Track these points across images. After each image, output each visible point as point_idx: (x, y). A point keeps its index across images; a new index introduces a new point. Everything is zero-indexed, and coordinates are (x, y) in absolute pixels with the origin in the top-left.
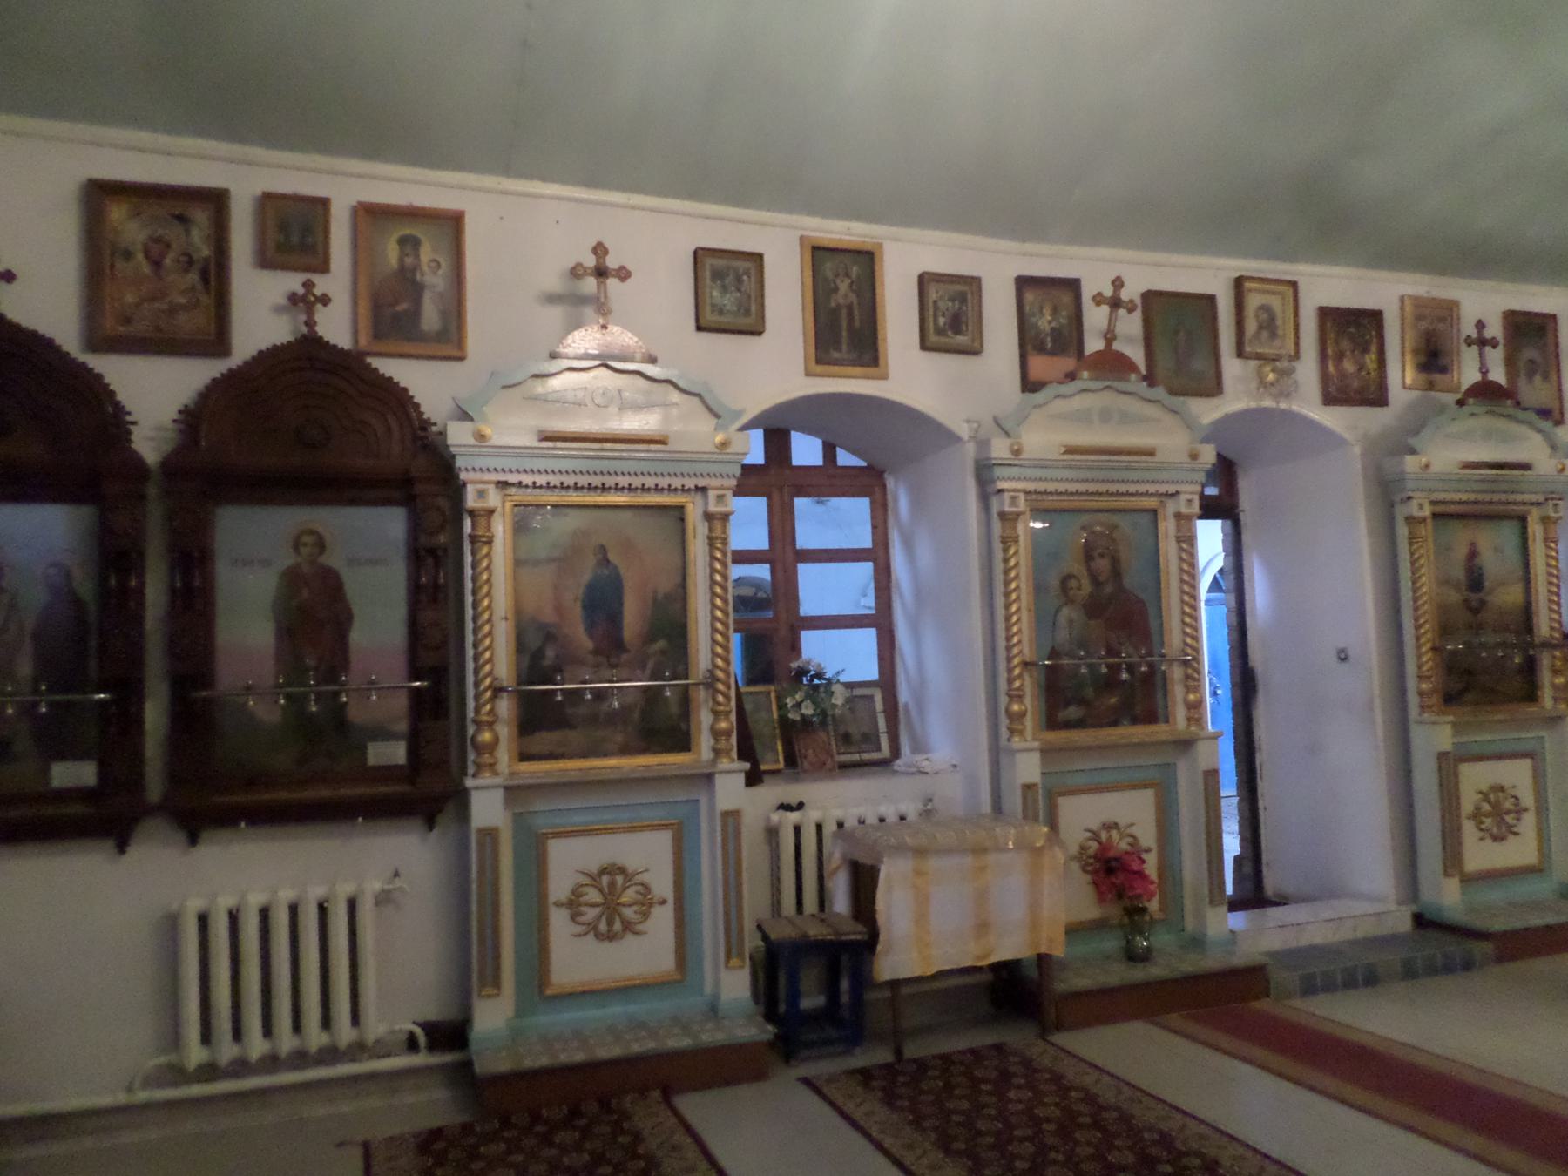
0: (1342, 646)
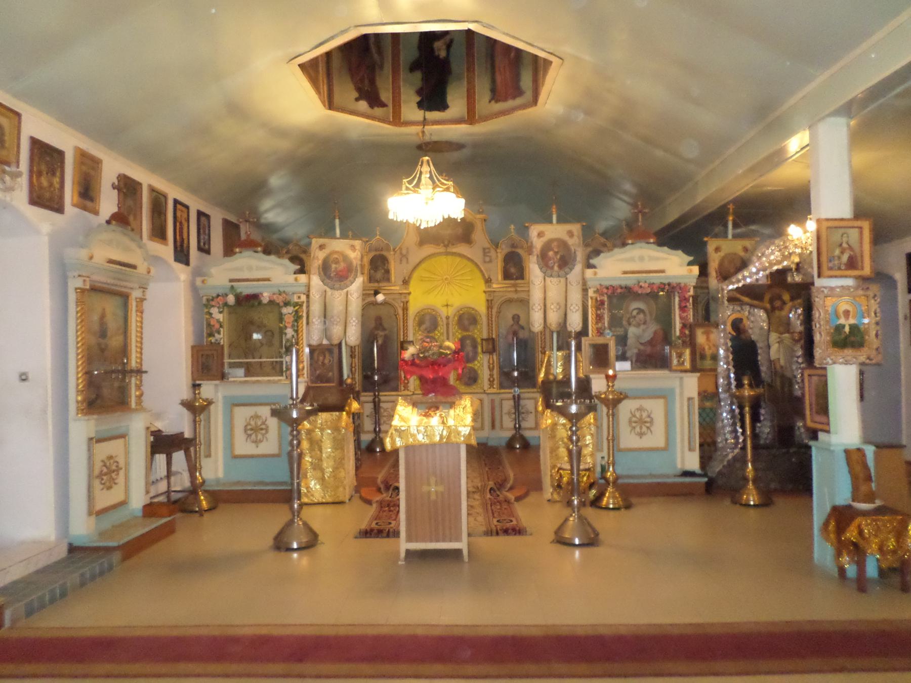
0: (23, 370)
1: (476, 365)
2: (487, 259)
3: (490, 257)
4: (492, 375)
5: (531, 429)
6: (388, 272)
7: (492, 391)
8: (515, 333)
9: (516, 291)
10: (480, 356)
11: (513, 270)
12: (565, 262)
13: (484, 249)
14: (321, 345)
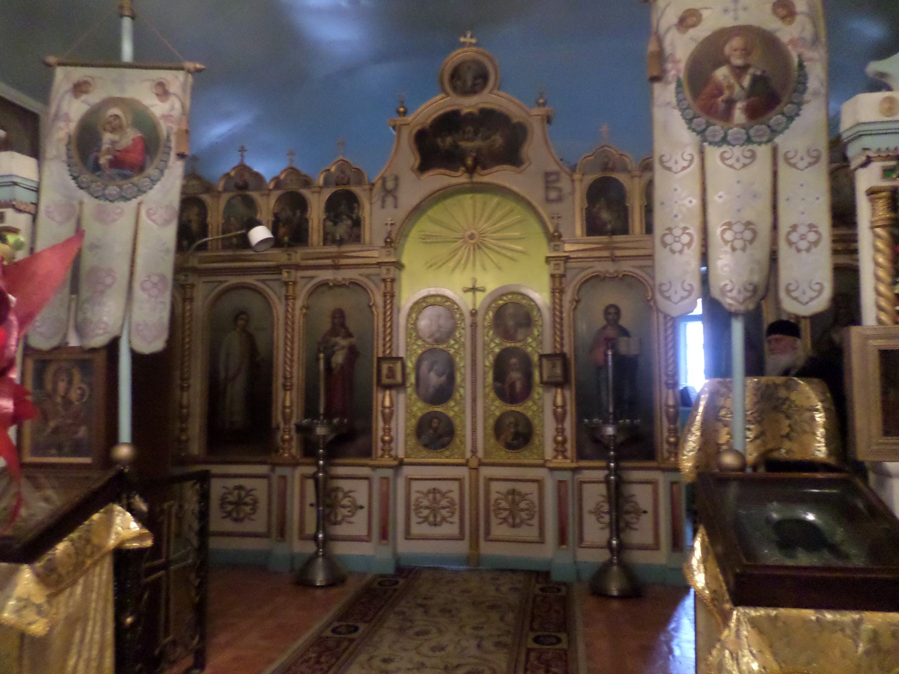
1: (527, 408)
2: (553, 195)
3: (560, 190)
4: (561, 431)
5: (643, 548)
6: (357, 223)
7: (560, 462)
8: (611, 343)
9: (614, 259)
10: (538, 391)
11: (605, 215)
12: (770, 97)
13: (547, 174)
14: (61, 348)
